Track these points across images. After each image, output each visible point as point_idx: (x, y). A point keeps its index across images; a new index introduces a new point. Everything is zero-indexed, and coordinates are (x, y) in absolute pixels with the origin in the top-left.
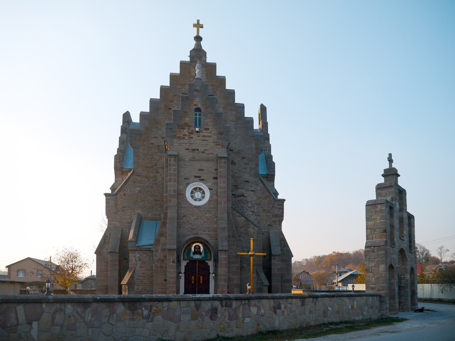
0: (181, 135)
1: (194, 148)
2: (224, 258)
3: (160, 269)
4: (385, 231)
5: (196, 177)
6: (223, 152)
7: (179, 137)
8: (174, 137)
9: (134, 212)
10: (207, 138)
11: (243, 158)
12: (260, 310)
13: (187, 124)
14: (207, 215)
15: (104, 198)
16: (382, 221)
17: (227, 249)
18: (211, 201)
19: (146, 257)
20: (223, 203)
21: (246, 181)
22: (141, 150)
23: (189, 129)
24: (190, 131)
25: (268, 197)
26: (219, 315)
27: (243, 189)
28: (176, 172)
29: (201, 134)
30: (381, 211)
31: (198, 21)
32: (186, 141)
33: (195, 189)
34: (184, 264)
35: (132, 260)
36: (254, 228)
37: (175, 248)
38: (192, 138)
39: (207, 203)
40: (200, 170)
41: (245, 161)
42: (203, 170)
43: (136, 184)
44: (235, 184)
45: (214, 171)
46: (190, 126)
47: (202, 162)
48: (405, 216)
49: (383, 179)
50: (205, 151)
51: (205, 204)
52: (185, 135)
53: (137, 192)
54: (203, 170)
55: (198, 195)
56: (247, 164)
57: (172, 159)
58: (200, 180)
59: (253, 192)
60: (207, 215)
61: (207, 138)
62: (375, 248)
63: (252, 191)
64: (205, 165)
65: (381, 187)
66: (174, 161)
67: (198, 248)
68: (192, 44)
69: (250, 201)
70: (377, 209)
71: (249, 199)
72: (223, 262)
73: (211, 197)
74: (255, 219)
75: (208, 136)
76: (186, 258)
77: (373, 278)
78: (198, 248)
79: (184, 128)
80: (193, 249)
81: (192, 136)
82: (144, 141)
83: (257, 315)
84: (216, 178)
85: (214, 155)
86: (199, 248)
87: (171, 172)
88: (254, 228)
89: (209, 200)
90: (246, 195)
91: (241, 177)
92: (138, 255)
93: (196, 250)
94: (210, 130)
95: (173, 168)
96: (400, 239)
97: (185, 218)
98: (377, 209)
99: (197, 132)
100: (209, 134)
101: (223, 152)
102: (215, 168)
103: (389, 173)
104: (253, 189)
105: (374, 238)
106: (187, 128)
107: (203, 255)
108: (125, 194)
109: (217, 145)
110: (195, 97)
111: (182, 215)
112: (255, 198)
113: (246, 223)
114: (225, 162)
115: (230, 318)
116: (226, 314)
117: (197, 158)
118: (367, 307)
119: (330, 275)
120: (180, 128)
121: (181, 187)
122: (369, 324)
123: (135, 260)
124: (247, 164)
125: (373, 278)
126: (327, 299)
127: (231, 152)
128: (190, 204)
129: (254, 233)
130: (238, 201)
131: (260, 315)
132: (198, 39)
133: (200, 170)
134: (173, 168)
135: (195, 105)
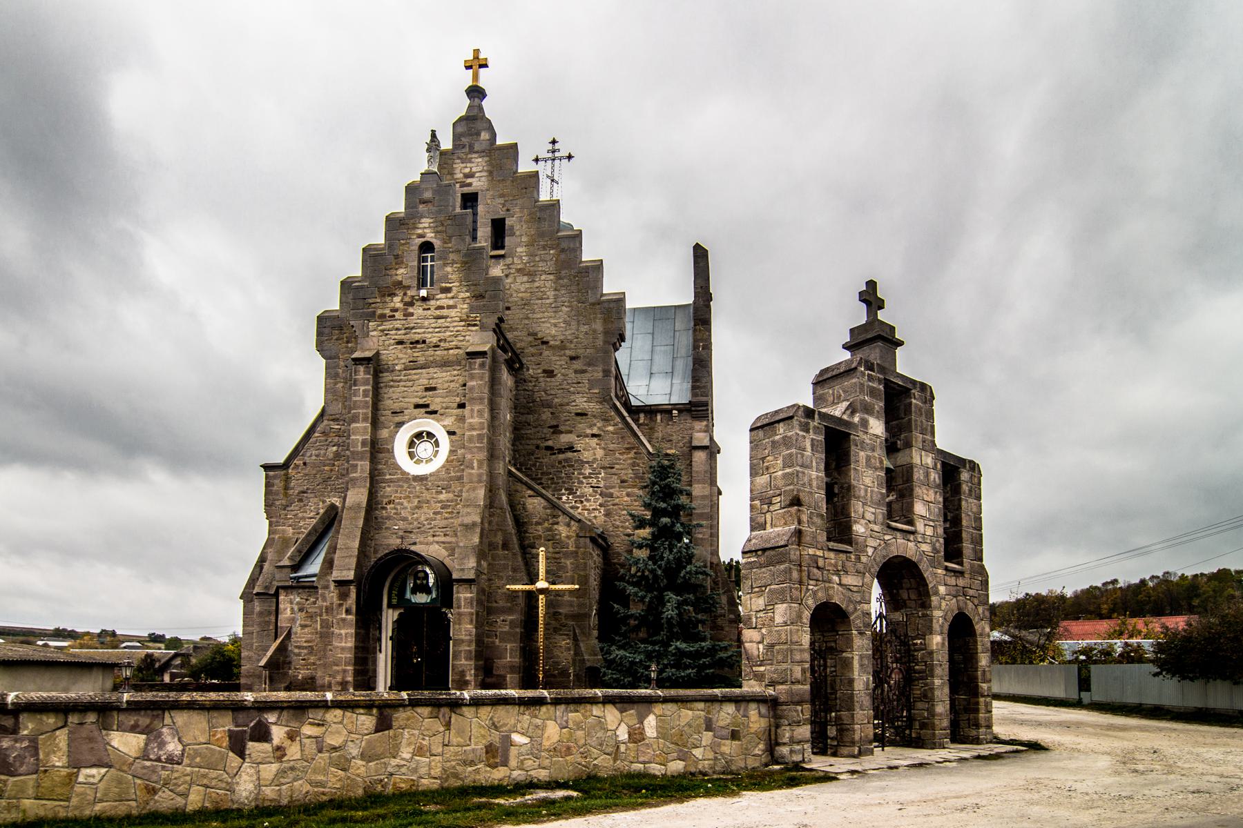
0: (387, 312)
1: (417, 337)
2: (466, 599)
5: (417, 406)
6: (482, 341)
7: (383, 316)
8: (372, 316)
10: (445, 312)
11: (572, 358)
12: (162, 745)
13: (401, 283)
14: (443, 496)
16: (788, 470)
17: (472, 576)
20: (475, 465)
21: (577, 414)
23: (405, 294)
24: (407, 299)
27: (571, 432)
31: (477, 52)
32: (398, 324)
33: (419, 435)
34: (390, 617)
38: (412, 314)
39: (443, 466)
40: (427, 389)
41: (577, 365)
42: (434, 389)
45: (460, 390)
46: (409, 287)
47: (431, 370)
48: (922, 460)
49: (847, 355)
51: (438, 471)
52: (396, 310)
53: (331, 456)
54: (434, 389)
55: (424, 449)
56: (584, 372)
57: (361, 368)
59: (595, 440)
60: (443, 496)
61: (445, 312)
63: (594, 436)
64: (442, 377)
66: (367, 372)
68: (462, 105)
70: (777, 438)
71: (586, 456)
73: (452, 452)
74: (601, 505)
75: (449, 307)
76: (394, 601)
77: (761, 646)
79: (395, 295)
81: (411, 310)
83: (145, 756)
84: (462, 406)
85: (461, 352)
88: (568, 525)
89: (447, 461)
91: (568, 404)
92: (298, 599)
94: (455, 290)
95: (362, 388)
96: (889, 527)
98: (777, 438)
99: (424, 299)
100: (451, 302)
101: (482, 341)
102: (461, 380)
104: (595, 431)
105: (768, 525)
108: (305, 464)
109: (469, 325)
110: (422, 217)
111: (385, 500)
112: (600, 453)
114: (482, 365)
117: (422, 360)
118: (707, 737)
119: (575, 639)
120: (384, 296)
121: (384, 433)
122: (726, 783)
123: (292, 609)
126: (514, 710)
128: (404, 473)
129: (568, 537)
130: (560, 462)
132: (476, 93)
133: (427, 389)
134: (362, 388)
135: (420, 236)
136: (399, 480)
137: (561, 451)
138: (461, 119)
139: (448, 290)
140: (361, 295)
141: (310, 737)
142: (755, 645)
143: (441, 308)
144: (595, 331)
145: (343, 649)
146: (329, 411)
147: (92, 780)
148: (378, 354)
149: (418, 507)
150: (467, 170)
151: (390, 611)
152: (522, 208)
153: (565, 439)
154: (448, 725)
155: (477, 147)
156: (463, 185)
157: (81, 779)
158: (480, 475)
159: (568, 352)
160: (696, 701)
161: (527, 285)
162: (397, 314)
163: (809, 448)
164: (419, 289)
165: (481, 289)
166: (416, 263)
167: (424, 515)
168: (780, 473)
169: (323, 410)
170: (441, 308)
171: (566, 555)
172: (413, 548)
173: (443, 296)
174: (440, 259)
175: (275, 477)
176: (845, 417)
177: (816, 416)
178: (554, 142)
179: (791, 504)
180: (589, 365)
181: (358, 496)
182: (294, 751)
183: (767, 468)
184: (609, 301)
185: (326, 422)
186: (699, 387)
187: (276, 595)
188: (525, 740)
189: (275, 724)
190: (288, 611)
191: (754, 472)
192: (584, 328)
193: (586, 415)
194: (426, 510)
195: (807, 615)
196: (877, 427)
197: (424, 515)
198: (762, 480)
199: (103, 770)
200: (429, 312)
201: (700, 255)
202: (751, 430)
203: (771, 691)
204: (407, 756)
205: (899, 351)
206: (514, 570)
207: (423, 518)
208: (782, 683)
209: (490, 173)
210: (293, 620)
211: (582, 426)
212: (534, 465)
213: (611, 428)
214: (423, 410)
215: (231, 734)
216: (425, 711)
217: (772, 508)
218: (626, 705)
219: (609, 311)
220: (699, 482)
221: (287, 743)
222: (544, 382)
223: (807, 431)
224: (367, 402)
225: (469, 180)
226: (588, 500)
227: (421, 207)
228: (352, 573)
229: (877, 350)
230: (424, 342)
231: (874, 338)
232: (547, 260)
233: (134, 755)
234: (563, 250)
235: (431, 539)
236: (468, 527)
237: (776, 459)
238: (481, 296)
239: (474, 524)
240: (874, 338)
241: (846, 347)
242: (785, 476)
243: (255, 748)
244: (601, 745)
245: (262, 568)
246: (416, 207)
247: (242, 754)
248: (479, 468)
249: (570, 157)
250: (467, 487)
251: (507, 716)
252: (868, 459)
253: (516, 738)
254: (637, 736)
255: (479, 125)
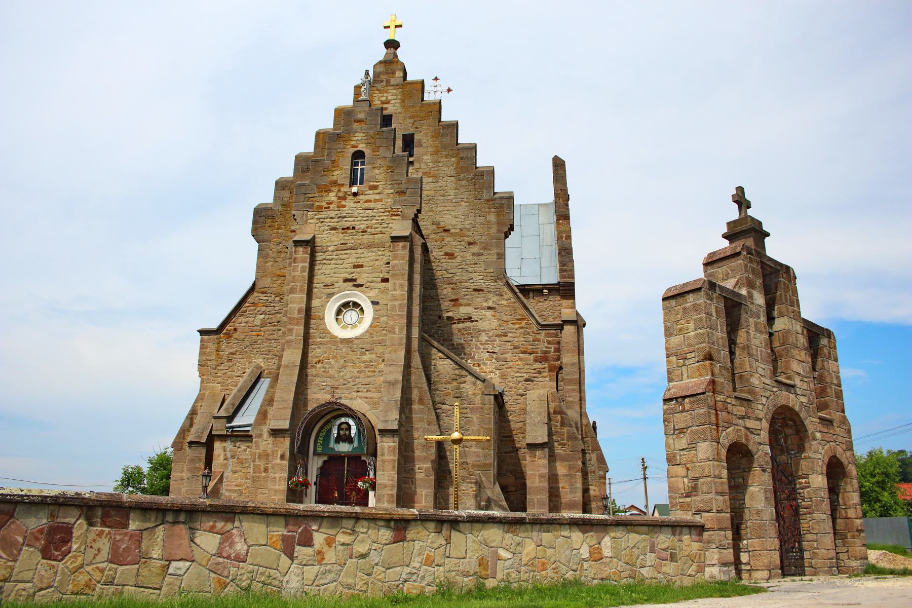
0: (324, 204)
1: (348, 224)
3: (264, 474)
4: (709, 357)
5: (346, 280)
6: (403, 228)
7: (320, 207)
8: (310, 208)
9: (250, 362)
10: (372, 205)
11: (470, 244)
12: (232, 544)
13: (336, 182)
14: (366, 357)
15: (198, 336)
17: (395, 427)
18: (375, 327)
19: (245, 450)
20: (397, 330)
21: (475, 290)
22: (272, 246)
23: (339, 191)
24: (341, 194)
25: (524, 319)
26: (75, 547)
27: (469, 305)
28: (306, 274)
29: (361, 198)
30: (696, 307)
33: (346, 305)
34: (315, 464)
35: (219, 456)
36: (475, 384)
37: (287, 427)
38: (344, 206)
39: (366, 332)
40: (356, 267)
41: (475, 249)
42: (362, 266)
43: (258, 309)
44: (454, 297)
46: (343, 185)
47: (359, 251)
49: (726, 243)
50: (369, 230)
51: (363, 335)
52: (331, 203)
53: (259, 323)
54: (362, 266)
55: (350, 316)
56: (479, 255)
57: (301, 249)
58: (354, 286)
59: (491, 312)
61: (372, 205)
62: (687, 400)
63: (489, 308)
65: (714, 259)
67: (346, 429)
68: (381, 53)
69: (484, 331)
71: (482, 325)
72: (386, 457)
75: (376, 201)
76: (319, 450)
78: (346, 429)
80: (335, 432)
82: (278, 229)
83: (219, 554)
84: (386, 280)
86: (349, 427)
87: (296, 274)
88: (475, 384)
90: (474, 318)
93: (342, 433)
95: (300, 265)
97: (320, 365)
99: (355, 194)
100: (377, 197)
102: (385, 259)
103: (738, 229)
104: (490, 304)
105: (685, 376)
106: (335, 189)
107: (356, 444)
109: (392, 215)
110: (355, 132)
111: (315, 360)
112: (495, 323)
113: (457, 372)
115: (116, 558)
116: (105, 545)
117: (351, 243)
124: (479, 255)
125: (686, 480)
127: (446, 234)
128: (333, 337)
131: (229, 557)
133: (356, 267)
134: (300, 265)
135: (354, 146)
136: (328, 343)
137: (460, 321)
138: (380, 62)
139: (375, 187)
140: (303, 191)
141: (343, 544)
142: (680, 479)
143: (369, 201)
144: (489, 222)
145: (276, 491)
146: (258, 285)
147: (179, 572)
148: (314, 237)
149: (344, 367)
150: (384, 99)
151: (316, 458)
152: (429, 126)
153: (463, 311)
154: (448, 540)
155: (393, 82)
156: (382, 109)
157: (171, 571)
158: (401, 339)
159: (466, 239)
160: (642, 525)
161: (432, 185)
162: (331, 206)
163: (714, 314)
164: (351, 186)
165: (403, 187)
166: (349, 167)
167: (347, 373)
168: (692, 333)
169: (254, 285)
170: (369, 201)
171: (473, 411)
172: (342, 401)
173: (371, 192)
174: (369, 163)
175: (209, 341)
176: (736, 290)
177: (717, 289)
178: (436, 79)
179: (705, 359)
180: (485, 249)
181: (293, 356)
182: (330, 556)
183: (680, 330)
184: (501, 198)
185: (255, 294)
186: (566, 271)
187: (209, 445)
188: (509, 555)
189: (317, 531)
190: (222, 457)
191: (668, 333)
192: (482, 220)
193: (482, 290)
194: (351, 369)
195: (724, 452)
196: (759, 299)
197: (347, 373)
198: (676, 340)
199: (188, 564)
200: (359, 205)
201: (559, 166)
202: (664, 299)
203: (698, 518)
204: (417, 565)
205: (767, 240)
206: (429, 423)
207: (348, 376)
208: (708, 512)
209: (403, 101)
210: (226, 466)
211: (479, 300)
212: (437, 333)
213: (504, 302)
214: (351, 284)
215: (285, 539)
216: (431, 526)
217: (687, 362)
218: (587, 527)
219: (501, 206)
220: (568, 351)
221: (326, 548)
222: (446, 263)
223: (712, 300)
224: (304, 277)
225: (385, 106)
226: (485, 364)
227: (356, 126)
228: (288, 422)
229: (751, 239)
230: (354, 228)
231: (747, 233)
232: (448, 167)
233: (213, 552)
234: (462, 158)
235: (355, 394)
236: (390, 384)
237: (688, 322)
238: (402, 193)
239: (396, 381)
240: (747, 233)
241: (725, 236)
242: (697, 336)
243: (301, 551)
244: (569, 562)
245: (192, 420)
246: (351, 125)
247: (291, 557)
248: (400, 333)
249: (449, 90)
250: (389, 349)
251: (494, 534)
252: (756, 324)
253: (503, 553)
254: (596, 556)
255: (394, 67)
